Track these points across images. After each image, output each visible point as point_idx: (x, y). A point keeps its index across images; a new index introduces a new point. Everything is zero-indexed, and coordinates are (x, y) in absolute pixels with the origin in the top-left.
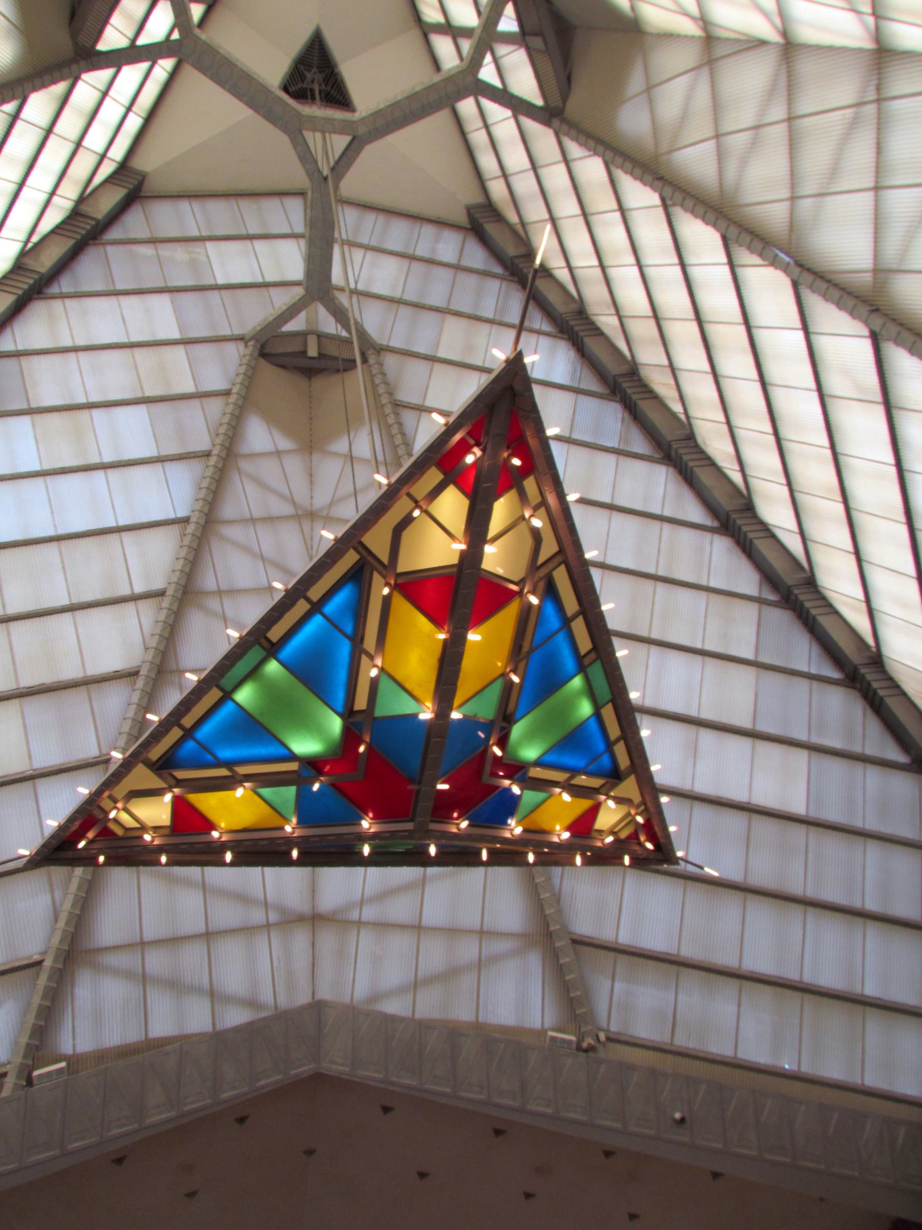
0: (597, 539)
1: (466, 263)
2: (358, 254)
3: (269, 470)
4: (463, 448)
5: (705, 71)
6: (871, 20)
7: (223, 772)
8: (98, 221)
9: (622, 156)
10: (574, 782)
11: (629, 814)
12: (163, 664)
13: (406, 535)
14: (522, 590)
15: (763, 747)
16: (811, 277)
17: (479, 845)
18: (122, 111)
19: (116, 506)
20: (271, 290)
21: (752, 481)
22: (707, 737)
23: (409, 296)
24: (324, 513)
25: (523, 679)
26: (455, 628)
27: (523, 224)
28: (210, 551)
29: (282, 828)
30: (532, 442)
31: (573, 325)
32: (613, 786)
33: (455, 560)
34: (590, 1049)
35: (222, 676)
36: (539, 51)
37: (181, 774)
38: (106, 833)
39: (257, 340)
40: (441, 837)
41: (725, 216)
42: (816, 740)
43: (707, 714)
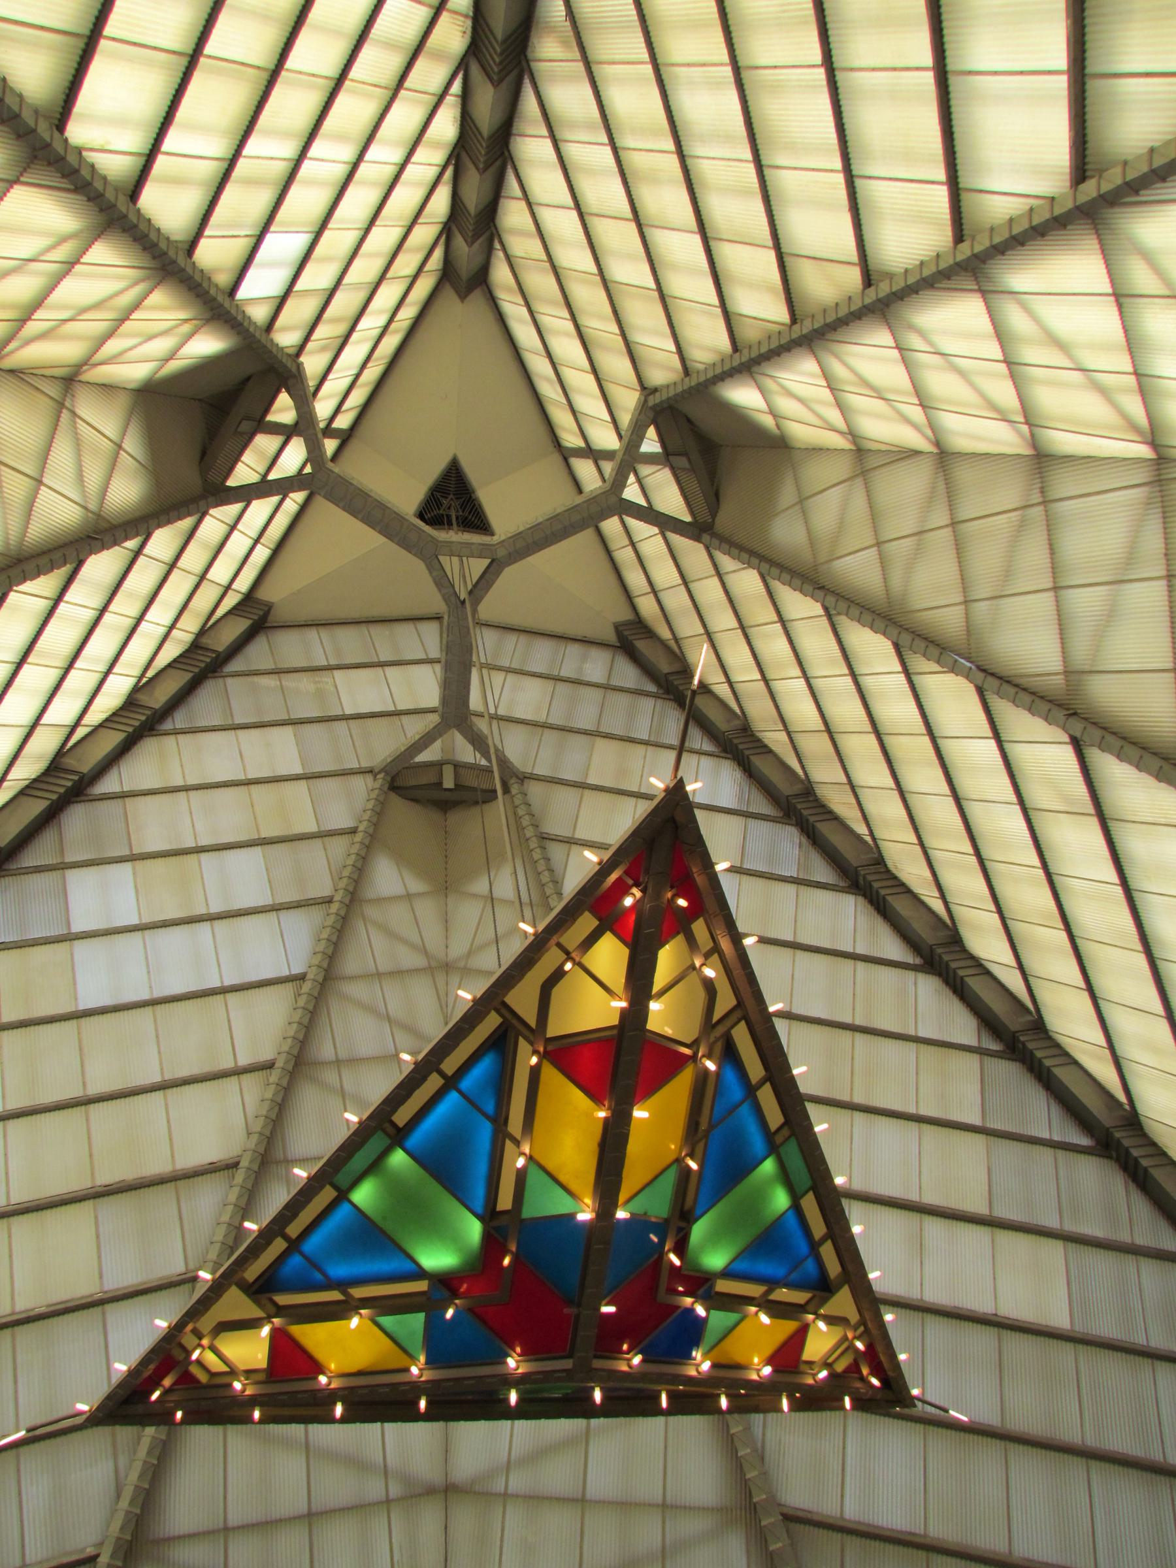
0: (782, 984)
1: (615, 682)
2: (498, 678)
3: (398, 916)
4: (621, 889)
5: (859, 482)
6: (1025, 429)
7: (335, 1295)
8: (218, 654)
9: (776, 566)
10: (772, 1297)
11: (845, 1338)
12: (268, 1155)
13: (556, 992)
14: (696, 1054)
16: (995, 682)
18: (250, 542)
20: (403, 717)
21: (953, 908)
22: (934, 1228)
24: (462, 964)
26: (616, 1105)
28: (329, 1013)
29: (407, 1370)
30: (700, 880)
31: (738, 744)
32: (824, 1301)
36: (684, 469)
37: (283, 1299)
38: (186, 1379)
40: (609, 1379)
41: (895, 623)
42: (1070, 1227)
43: (930, 1198)
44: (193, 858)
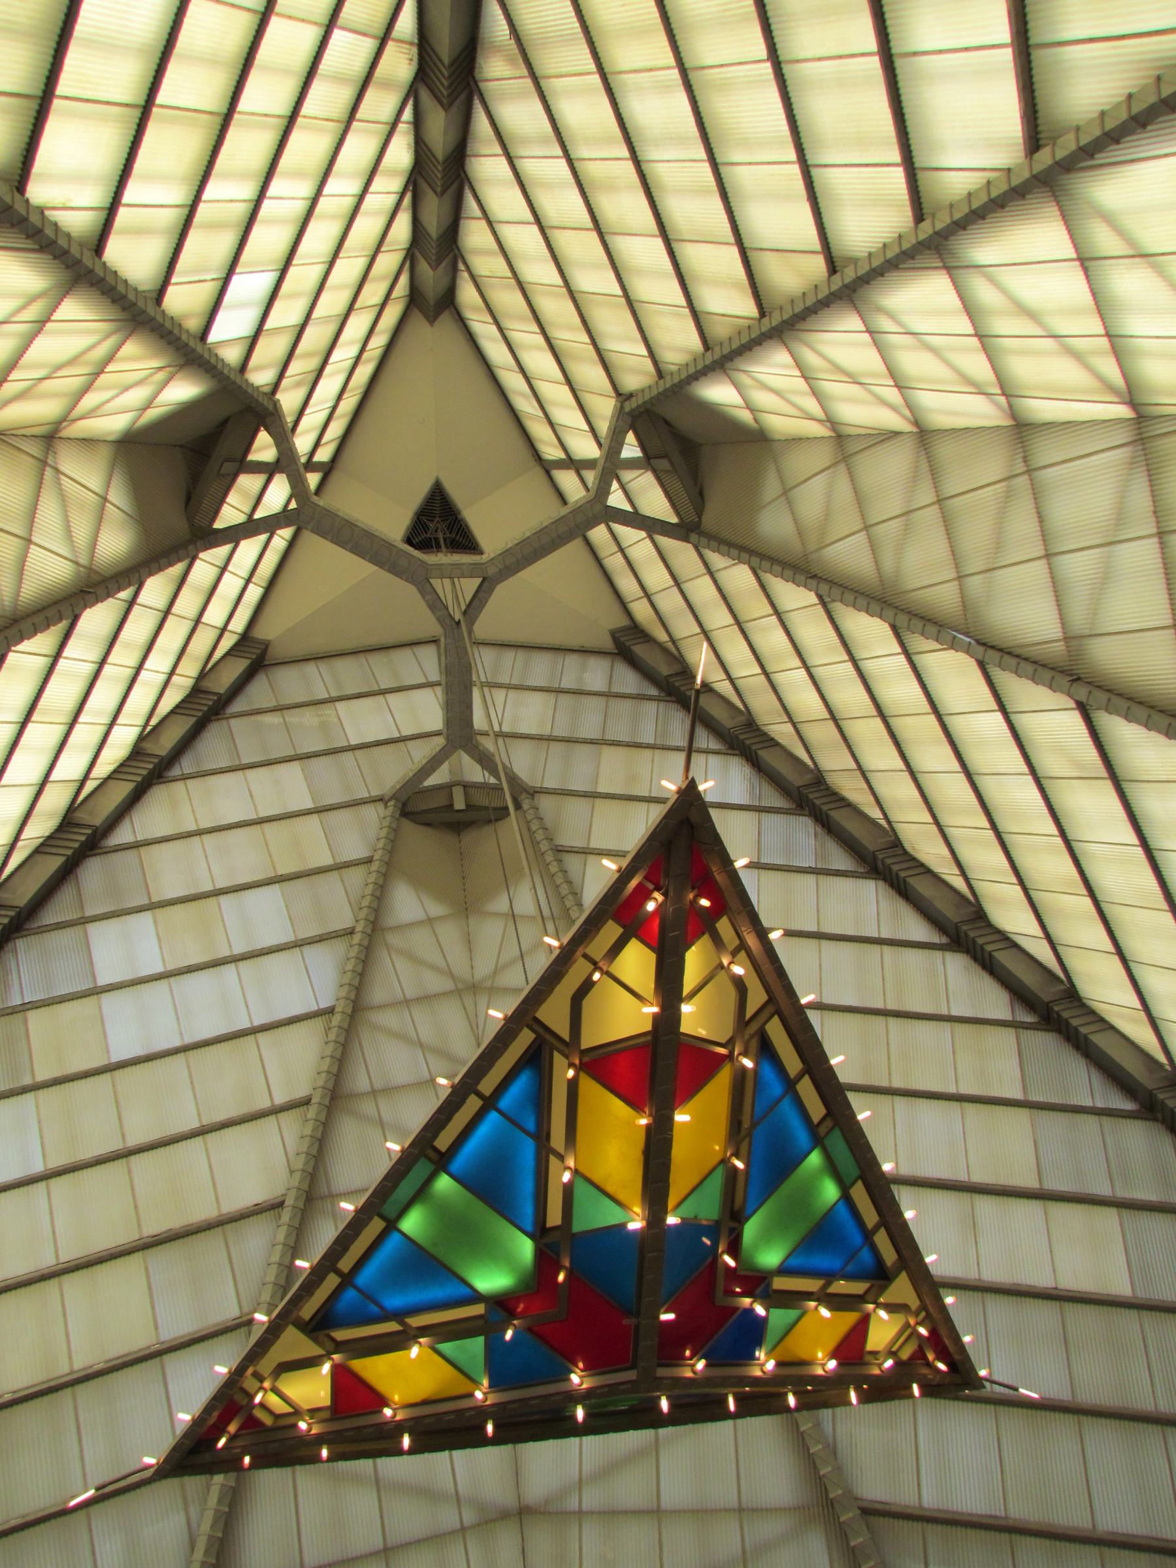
0: (813, 976)
1: (616, 689)
2: (499, 695)
3: (420, 942)
4: (642, 894)
5: (842, 468)
6: (1002, 399)
7: (392, 1326)
9: (765, 559)
10: (831, 1290)
12: (312, 1192)
13: (586, 1003)
14: (731, 1053)
15: (1060, 1211)
16: (995, 654)
17: (724, 1391)
18: (241, 583)
19: (249, 1002)
22: (985, 1206)
23: (559, 732)
24: (488, 984)
25: (748, 1164)
27: (673, 641)
30: (720, 878)
31: (745, 740)
32: (882, 1290)
33: (648, 1027)
35: (384, 1201)
37: (341, 1335)
38: (251, 1423)
39: (397, 800)
42: (1122, 1193)
43: (979, 1177)
44: (212, 901)
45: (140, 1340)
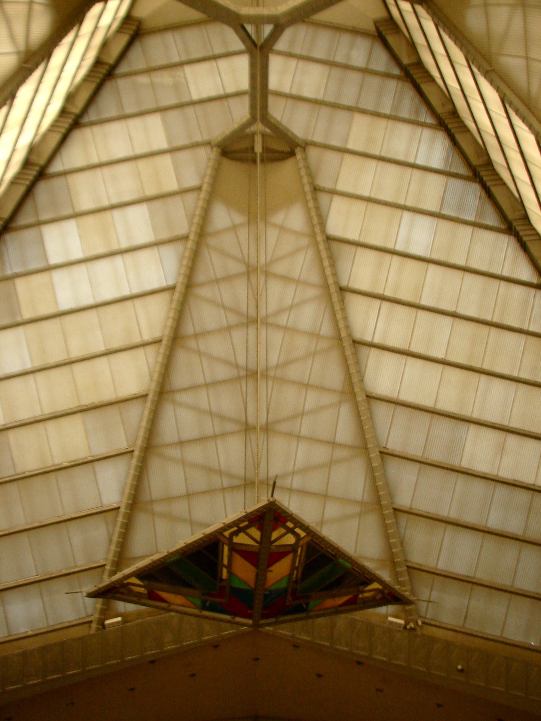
23: (330, 99)
34: (411, 629)
43: (515, 424)
45: (82, 454)
